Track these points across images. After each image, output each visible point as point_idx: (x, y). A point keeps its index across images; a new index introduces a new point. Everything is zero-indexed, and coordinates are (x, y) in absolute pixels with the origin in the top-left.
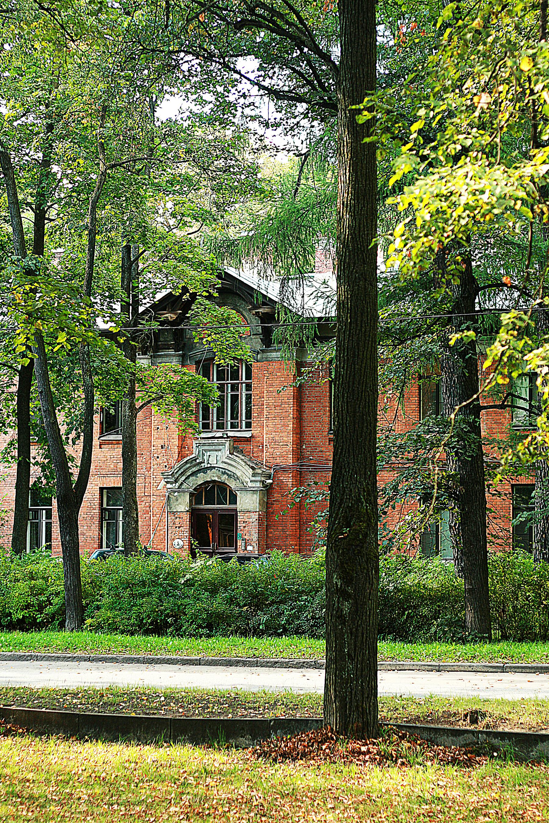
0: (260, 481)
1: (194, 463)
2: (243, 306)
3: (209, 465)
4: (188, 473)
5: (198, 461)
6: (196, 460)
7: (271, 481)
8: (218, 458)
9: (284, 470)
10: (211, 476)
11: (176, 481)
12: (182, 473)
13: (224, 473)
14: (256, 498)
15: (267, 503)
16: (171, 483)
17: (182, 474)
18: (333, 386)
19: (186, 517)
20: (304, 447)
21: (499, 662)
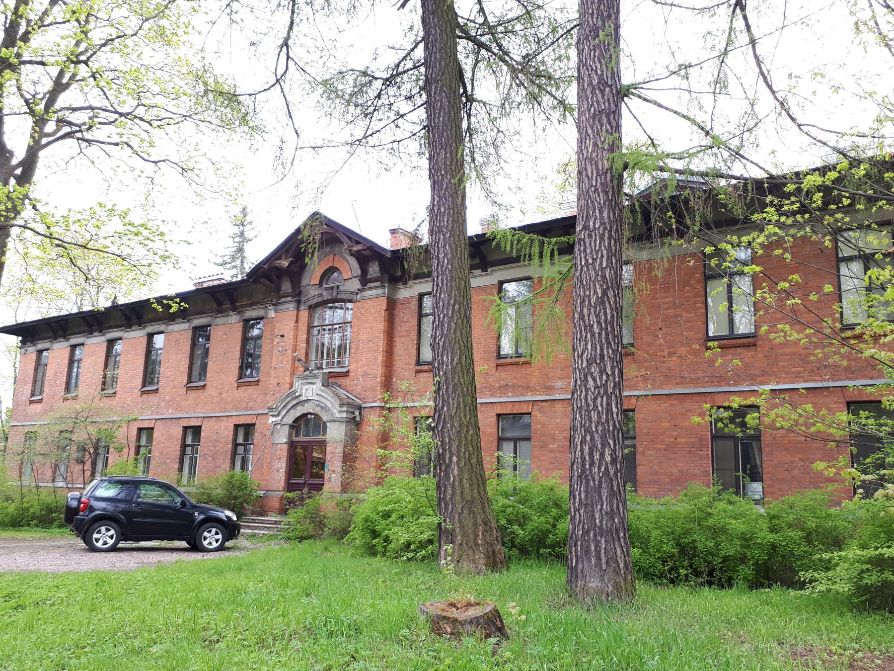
0: (347, 412)
10: (307, 408)
11: (278, 415)
13: (318, 405)
19: (285, 447)
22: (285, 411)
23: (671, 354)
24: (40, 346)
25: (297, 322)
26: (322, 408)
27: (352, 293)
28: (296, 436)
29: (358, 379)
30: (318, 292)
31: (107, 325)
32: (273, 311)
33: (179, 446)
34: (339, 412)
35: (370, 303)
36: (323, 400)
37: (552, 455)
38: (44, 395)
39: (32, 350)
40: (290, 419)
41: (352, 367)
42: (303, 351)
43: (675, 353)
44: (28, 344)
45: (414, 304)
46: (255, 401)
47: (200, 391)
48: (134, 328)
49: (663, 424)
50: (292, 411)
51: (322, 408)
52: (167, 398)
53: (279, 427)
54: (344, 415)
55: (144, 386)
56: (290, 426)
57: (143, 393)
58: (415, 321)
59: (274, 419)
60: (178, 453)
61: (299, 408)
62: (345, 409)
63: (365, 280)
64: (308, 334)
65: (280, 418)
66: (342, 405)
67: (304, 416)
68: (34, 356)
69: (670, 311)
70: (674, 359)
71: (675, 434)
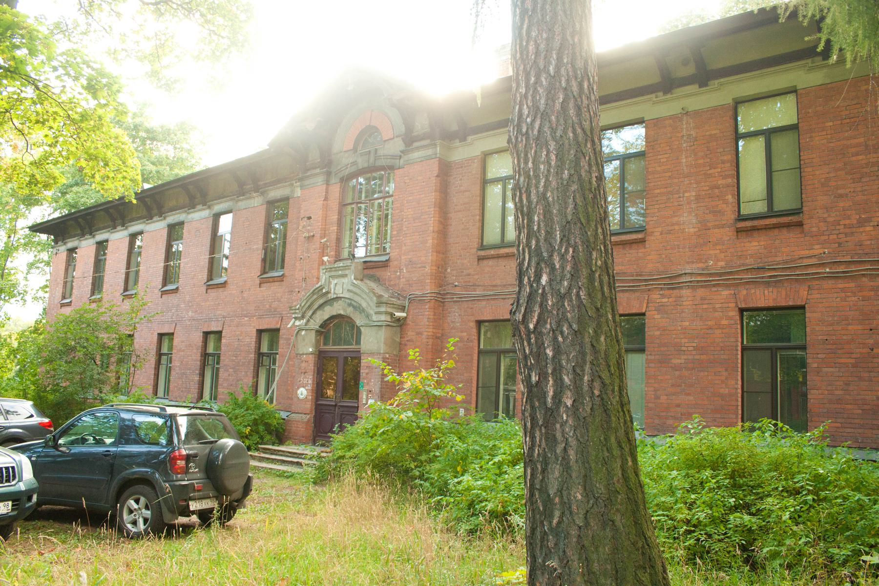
0: (386, 313)
1: (320, 293)
4: (316, 307)
5: (324, 291)
7: (404, 315)
10: (338, 309)
13: (350, 305)
14: (383, 334)
15: (400, 344)
18: (526, 21)
19: (312, 359)
20: (449, 270)
21: (639, 489)
23: (862, 223)
24: (71, 244)
25: (326, 199)
26: (354, 307)
27: (394, 157)
28: (325, 344)
29: (401, 270)
30: (351, 160)
31: (130, 217)
32: (299, 189)
33: (199, 355)
34: (376, 313)
36: (357, 298)
37: (677, 373)
38: (73, 296)
39: (63, 249)
40: (315, 324)
41: (393, 255)
42: (334, 236)
43: (868, 220)
44: (60, 243)
45: (476, 166)
47: (221, 289)
48: (155, 219)
49: (850, 327)
50: (319, 313)
51: (354, 307)
52: (188, 298)
53: (303, 333)
54: (383, 317)
55: (164, 284)
56: (317, 331)
57: (164, 293)
58: (477, 189)
59: (297, 323)
60: (199, 363)
61: (327, 308)
62: (383, 309)
64: (340, 213)
65: (305, 320)
66: (379, 303)
67: (332, 318)
68: (63, 255)
69: (860, 157)
70: (868, 229)
71: (871, 341)
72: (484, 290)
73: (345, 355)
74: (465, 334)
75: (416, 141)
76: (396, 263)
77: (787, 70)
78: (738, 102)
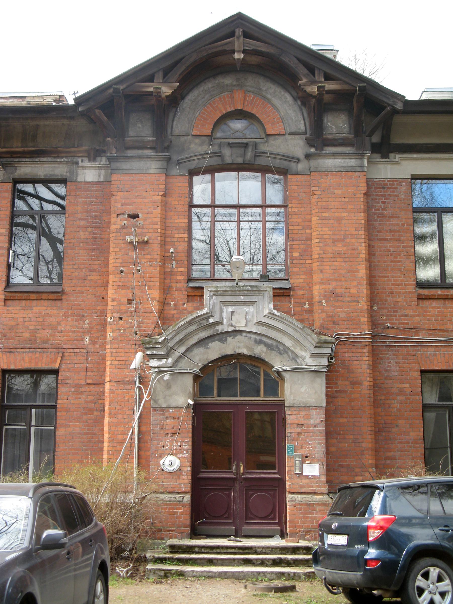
1: (204, 323)
2: (271, 91)
3: (231, 329)
5: (211, 320)
6: (208, 318)
8: (249, 317)
9: (355, 342)
10: (233, 346)
11: (167, 356)
12: (181, 340)
13: (260, 342)
16: (159, 357)
17: (181, 342)
22: (182, 349)
34: (314, 355)
35: (331, 179)
46: (54, 328)
53: (167, 377)
63: (318, 139)
67: (225, 358)
72: (430, 335)
73: (248, 409)
74: (407, 385)
75: (328, 145)
76: (301, 293)
77: (422, 159)
78: (414, 178)
